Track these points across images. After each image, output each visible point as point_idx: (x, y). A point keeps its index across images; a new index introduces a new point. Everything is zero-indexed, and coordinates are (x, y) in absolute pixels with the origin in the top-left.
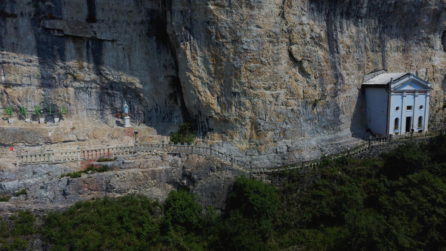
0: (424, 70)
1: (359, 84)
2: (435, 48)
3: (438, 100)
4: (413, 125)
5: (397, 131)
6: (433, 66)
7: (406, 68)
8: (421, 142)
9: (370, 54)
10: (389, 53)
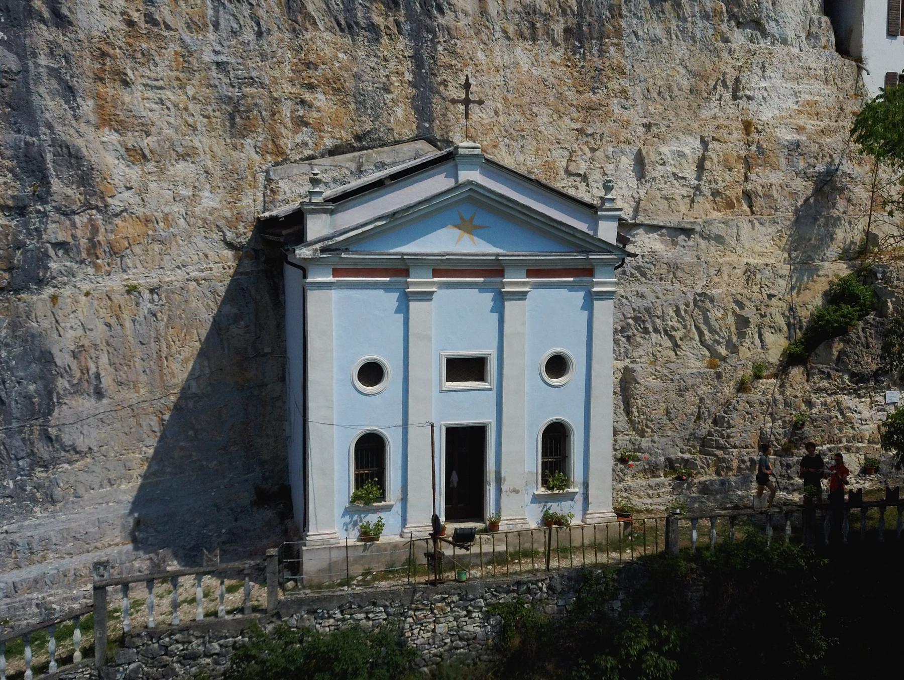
0: (690, 146)
1: (239, 217)
2: (771, 27)
3: (754, 319)
4: (499, 480)
5: (372, 519)
6: (748, 126)
7: (581, 131)
8: (504, 598)
9: (325, 42)
10: (470, 46)
